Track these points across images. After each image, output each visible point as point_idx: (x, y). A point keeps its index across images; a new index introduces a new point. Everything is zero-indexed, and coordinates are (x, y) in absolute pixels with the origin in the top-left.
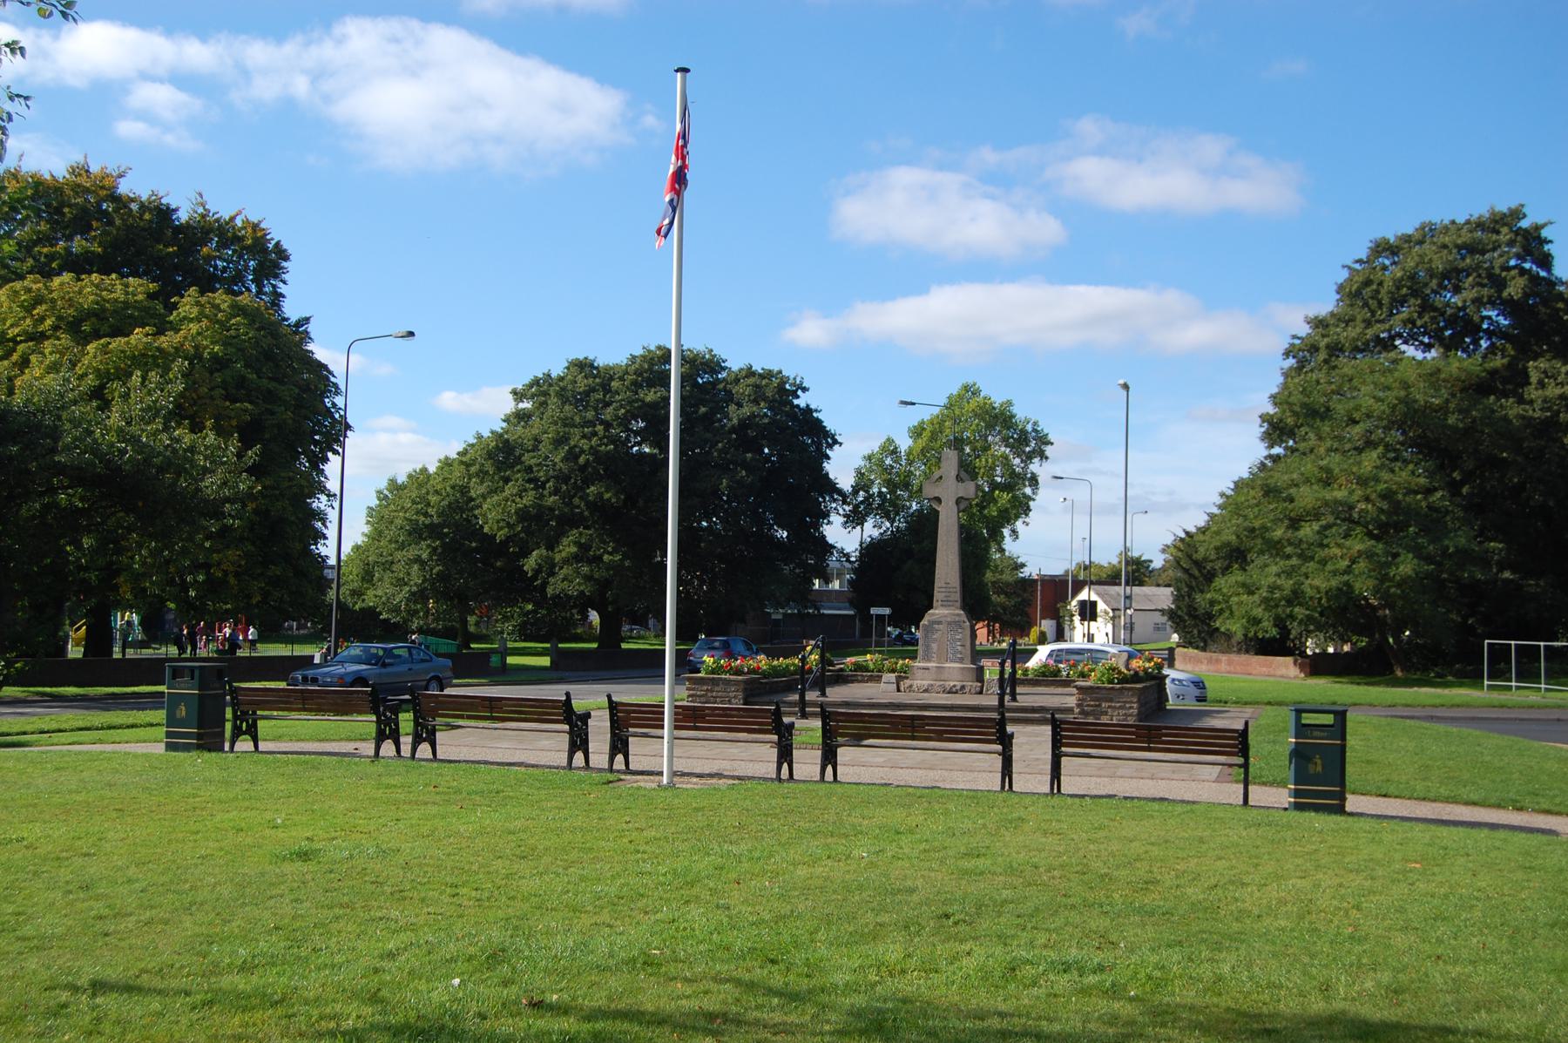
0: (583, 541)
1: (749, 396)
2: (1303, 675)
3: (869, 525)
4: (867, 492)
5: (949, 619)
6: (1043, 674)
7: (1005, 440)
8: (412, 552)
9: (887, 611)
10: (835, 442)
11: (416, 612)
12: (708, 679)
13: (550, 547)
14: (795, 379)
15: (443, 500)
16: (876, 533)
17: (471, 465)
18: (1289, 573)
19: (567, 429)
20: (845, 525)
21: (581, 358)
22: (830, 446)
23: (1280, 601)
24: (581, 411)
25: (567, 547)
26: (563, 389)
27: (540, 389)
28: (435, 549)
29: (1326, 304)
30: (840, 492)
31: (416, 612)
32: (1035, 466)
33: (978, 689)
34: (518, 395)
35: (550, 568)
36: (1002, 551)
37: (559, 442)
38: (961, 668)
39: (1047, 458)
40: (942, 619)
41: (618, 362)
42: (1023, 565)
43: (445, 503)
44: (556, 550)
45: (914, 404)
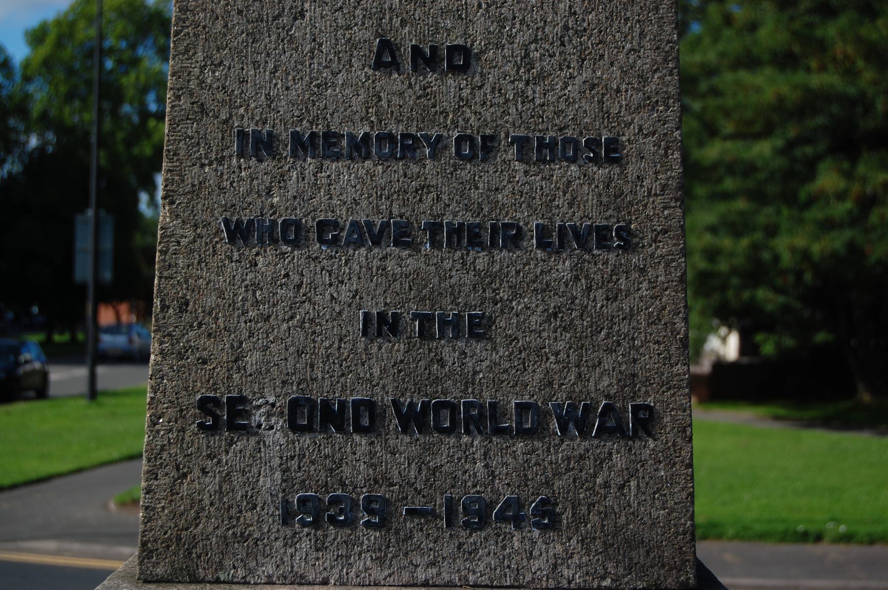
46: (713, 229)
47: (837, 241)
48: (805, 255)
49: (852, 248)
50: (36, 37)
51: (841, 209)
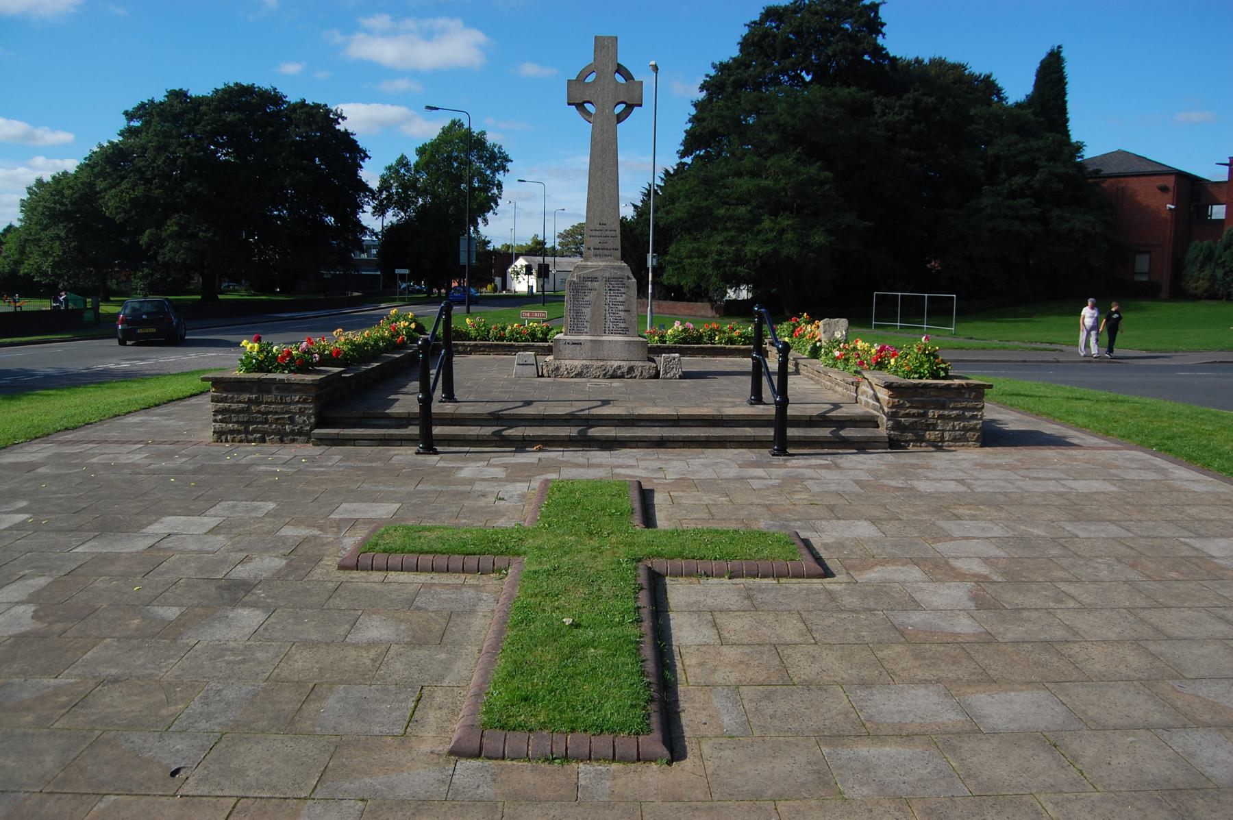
0: (183, 222)
1: (304, 120)
2: (718, 316)
3: (390, 213)
4: (388, 191)
5: (607, 274)
6: (684, 341)
7: (480, 158)
8: (52, 232)
9: (407, 271)
10: (366, 156)
11: (62, 276)
12: (251, 381)
13: (159, 227)
14: (336, 110)
15: (75, 193)
16: (395, 220)
17: (95, 167)
18: (730, 242)
19: (166, 140)
20: (373, 214)
21: (177, 89)
22: (363, 159)
23: (726, 262)
24: (178, 127)
25: (171, 227)
26: (162, 110)
27: (144, 111)
28: (70, 229)
29: (731, 52)
30: (371, 190)
31: (62, 276)
32: (500, 176)
33: (653, 372)
34: (130, 116)
35: (159, 242)
36: (477, 232)
37: (162, 148)
38: (591, 341)
39: (508, 171)
40: (596, 275)
41: (205, 94)
42: (489, 242)
43: (77, 195)
44: (163, 229)
45: (437, 109)
46: (721, 243)
47: (768, 248)
48: (756, 253)
49: (775, 250)
50: (421, 151)
51: (771, 235)
